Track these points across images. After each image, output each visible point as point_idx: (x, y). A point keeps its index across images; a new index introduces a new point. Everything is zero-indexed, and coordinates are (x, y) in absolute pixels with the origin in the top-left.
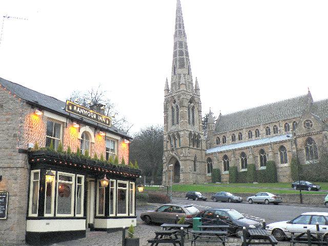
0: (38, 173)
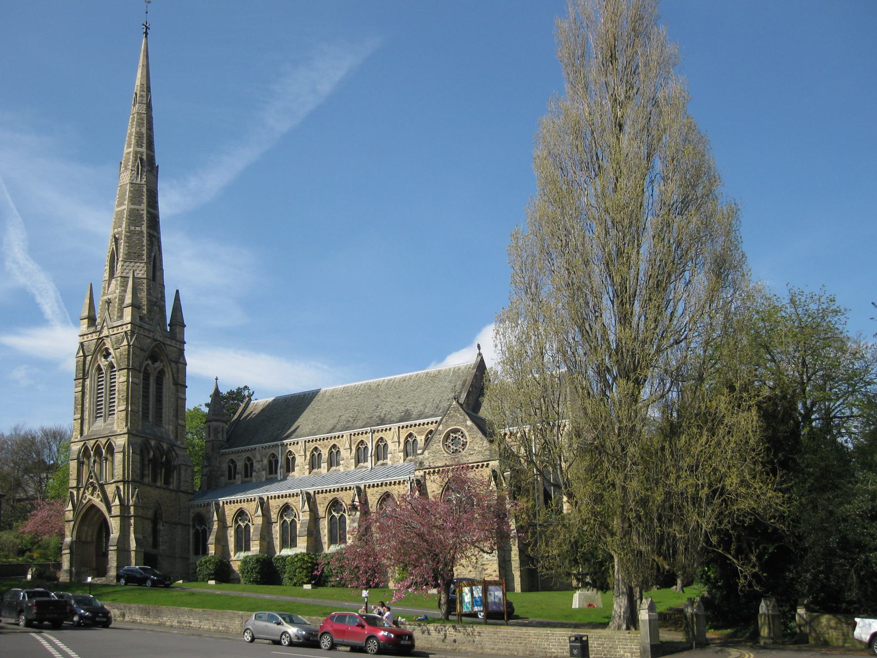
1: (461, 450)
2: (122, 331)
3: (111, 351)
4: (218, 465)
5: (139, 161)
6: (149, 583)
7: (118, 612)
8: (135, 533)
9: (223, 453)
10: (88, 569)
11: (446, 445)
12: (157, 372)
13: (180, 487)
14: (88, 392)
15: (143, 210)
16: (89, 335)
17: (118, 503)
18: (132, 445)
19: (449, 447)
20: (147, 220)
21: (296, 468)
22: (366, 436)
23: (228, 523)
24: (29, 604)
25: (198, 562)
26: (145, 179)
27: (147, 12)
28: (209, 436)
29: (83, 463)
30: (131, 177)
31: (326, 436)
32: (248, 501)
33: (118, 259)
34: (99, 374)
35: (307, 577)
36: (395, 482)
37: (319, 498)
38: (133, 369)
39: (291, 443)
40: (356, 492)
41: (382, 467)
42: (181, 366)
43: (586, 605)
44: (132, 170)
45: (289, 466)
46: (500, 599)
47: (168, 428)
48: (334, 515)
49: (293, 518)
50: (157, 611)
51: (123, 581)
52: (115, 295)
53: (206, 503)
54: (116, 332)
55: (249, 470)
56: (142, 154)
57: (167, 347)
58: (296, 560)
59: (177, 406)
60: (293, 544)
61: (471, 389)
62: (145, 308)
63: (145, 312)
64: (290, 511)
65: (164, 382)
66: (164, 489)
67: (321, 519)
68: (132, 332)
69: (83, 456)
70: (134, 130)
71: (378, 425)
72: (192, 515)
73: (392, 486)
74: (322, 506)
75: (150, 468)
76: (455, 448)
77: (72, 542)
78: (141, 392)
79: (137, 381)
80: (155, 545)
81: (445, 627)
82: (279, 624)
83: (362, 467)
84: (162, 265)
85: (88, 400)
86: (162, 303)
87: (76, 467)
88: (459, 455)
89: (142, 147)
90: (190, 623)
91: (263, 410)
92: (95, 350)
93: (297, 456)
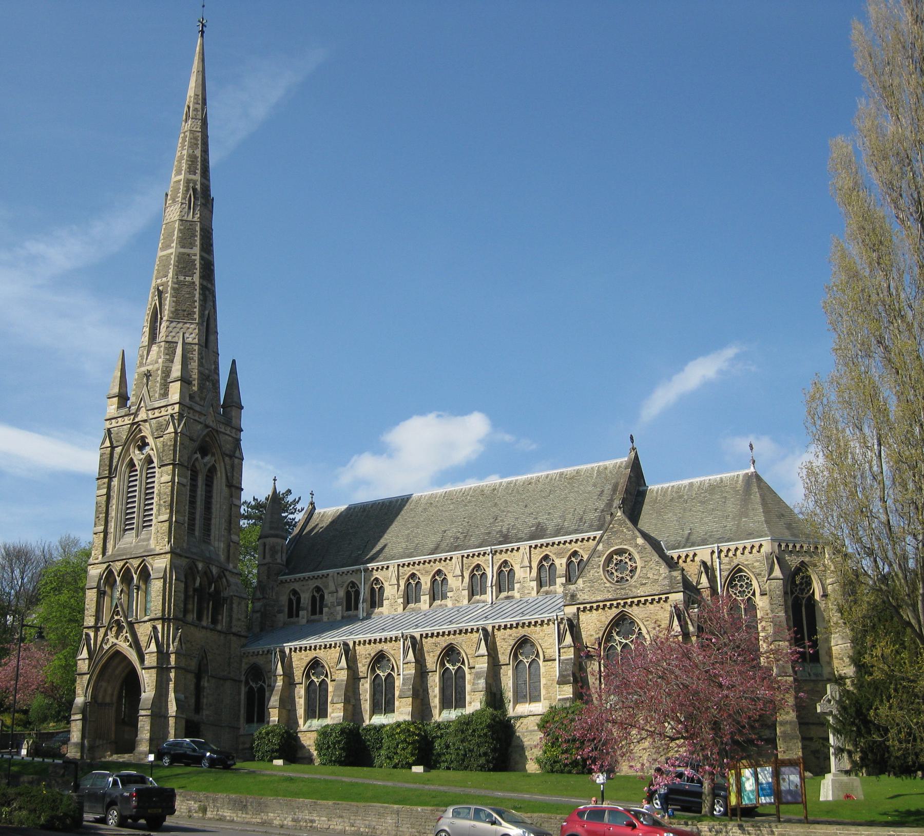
0: (446, 704)
1: (628, 578)
2: (166, 413)
3: (150, 440)
4: (274, 597)
5: (191, 192)
6: (205, 763)
7: (196, 805)
8: (175, 692)
9: (282, 581)
10: (105, 742)
11: (608, 571)
12: (207, 470)
13: (231, 627)
14: (115, 496)
15: (195, 255)
16: (119, 419)
17: (155, 650)
18: (176, 568)
19: (612, 573)
20: (201, 268)
21: (385, 602)
22: (484, 558)
23: (296, 678)
24: (126, 794)
25: (256, 734)
26: (198, 215)
27: (203, 6)
28: (264, 558)
29: (104, 593)
30: (181, 212)
31: (427, 558)
32: (325, 648)
33: (161, 318)
34: (131, 472)
35: (413, 755)
36: (536, 622)
37: (428, 643)
38: (181, 465)
39: (378, 568)
40: (482, 635)
41: (507, 602)
42: (236, 461)
43: (842, 796)
44: (182, 204)
45: (376, 598)
46: (797, 786)
47: (218, 546)
48: (448, 668)
49: (389, 671)
50: (260, 804)
51: (166, 760)
52: (156, 366)
53: (266, 650)
54: (157, 415)
55: (317, 605)
56: (195, 182)
57: (221, 436)
58: (398, 731)
59: (230, 516)
60: (389, 708)
61: (625, 496)
62: (196, 383)
63: (195, 388)
64: (385, 662)
65: (215, 482)
66: (211, 630)
67: (430, 674)
68: (181, 415)
69: (105, 585)
70: (185, 152)
71: (500, 543)
72: (244, 667)
73: (532, 627)
74: (431, 654)
75: (196, 600)
76: (620, 576)
77: (85, 704)
78: (188, 496)
79: (184, 481)
80: (198, 709)
81: (726, 826)
82: (494, 823)
83: (478, 602)
84: (216, 326)
85: (114, 507)
86: (216, 377)
87: (95, 599)
88: (626, 585)
89: (195, 174)
90: (312, 821)
91: (333, 522)
92: (127, 439)
93: (386, 585)
